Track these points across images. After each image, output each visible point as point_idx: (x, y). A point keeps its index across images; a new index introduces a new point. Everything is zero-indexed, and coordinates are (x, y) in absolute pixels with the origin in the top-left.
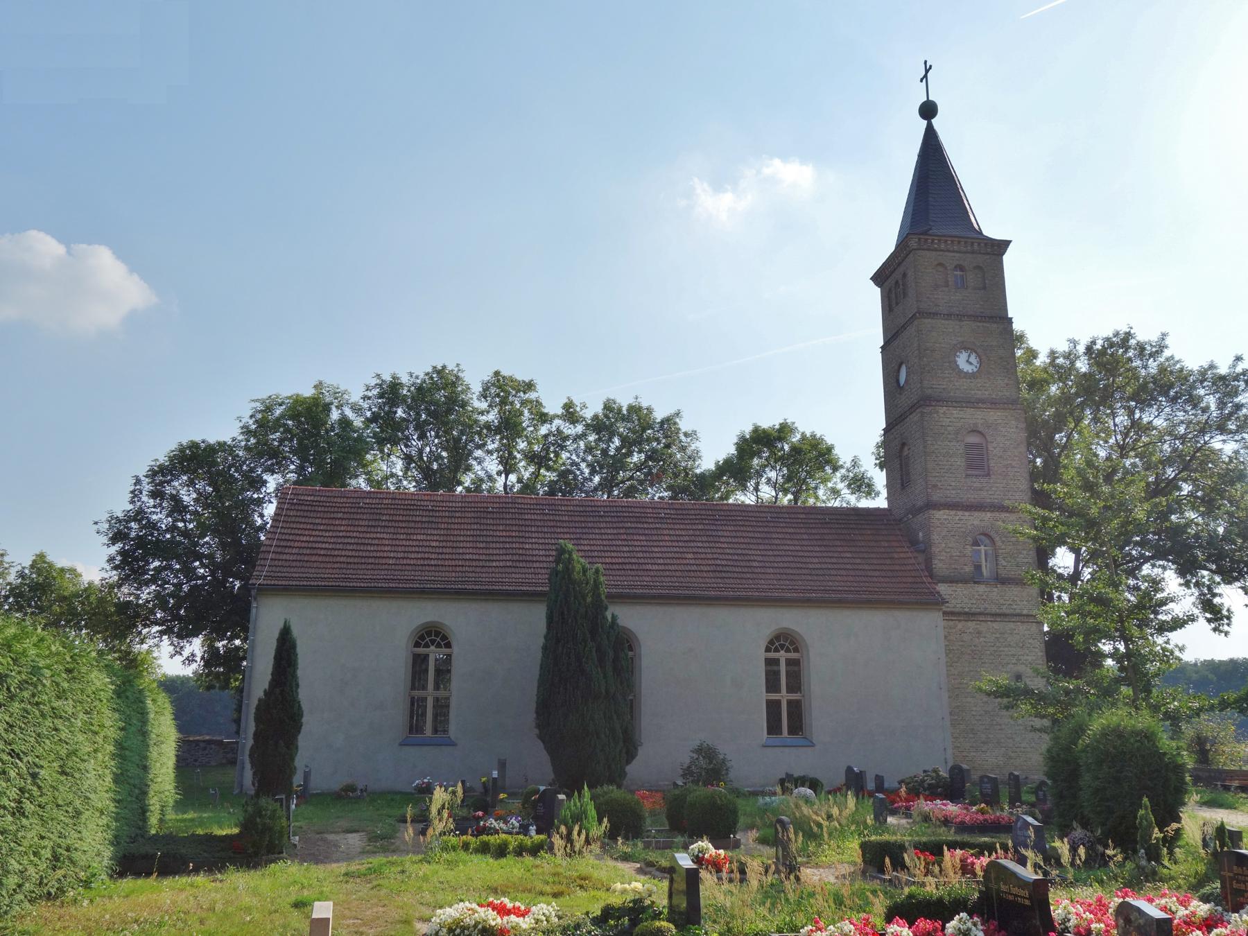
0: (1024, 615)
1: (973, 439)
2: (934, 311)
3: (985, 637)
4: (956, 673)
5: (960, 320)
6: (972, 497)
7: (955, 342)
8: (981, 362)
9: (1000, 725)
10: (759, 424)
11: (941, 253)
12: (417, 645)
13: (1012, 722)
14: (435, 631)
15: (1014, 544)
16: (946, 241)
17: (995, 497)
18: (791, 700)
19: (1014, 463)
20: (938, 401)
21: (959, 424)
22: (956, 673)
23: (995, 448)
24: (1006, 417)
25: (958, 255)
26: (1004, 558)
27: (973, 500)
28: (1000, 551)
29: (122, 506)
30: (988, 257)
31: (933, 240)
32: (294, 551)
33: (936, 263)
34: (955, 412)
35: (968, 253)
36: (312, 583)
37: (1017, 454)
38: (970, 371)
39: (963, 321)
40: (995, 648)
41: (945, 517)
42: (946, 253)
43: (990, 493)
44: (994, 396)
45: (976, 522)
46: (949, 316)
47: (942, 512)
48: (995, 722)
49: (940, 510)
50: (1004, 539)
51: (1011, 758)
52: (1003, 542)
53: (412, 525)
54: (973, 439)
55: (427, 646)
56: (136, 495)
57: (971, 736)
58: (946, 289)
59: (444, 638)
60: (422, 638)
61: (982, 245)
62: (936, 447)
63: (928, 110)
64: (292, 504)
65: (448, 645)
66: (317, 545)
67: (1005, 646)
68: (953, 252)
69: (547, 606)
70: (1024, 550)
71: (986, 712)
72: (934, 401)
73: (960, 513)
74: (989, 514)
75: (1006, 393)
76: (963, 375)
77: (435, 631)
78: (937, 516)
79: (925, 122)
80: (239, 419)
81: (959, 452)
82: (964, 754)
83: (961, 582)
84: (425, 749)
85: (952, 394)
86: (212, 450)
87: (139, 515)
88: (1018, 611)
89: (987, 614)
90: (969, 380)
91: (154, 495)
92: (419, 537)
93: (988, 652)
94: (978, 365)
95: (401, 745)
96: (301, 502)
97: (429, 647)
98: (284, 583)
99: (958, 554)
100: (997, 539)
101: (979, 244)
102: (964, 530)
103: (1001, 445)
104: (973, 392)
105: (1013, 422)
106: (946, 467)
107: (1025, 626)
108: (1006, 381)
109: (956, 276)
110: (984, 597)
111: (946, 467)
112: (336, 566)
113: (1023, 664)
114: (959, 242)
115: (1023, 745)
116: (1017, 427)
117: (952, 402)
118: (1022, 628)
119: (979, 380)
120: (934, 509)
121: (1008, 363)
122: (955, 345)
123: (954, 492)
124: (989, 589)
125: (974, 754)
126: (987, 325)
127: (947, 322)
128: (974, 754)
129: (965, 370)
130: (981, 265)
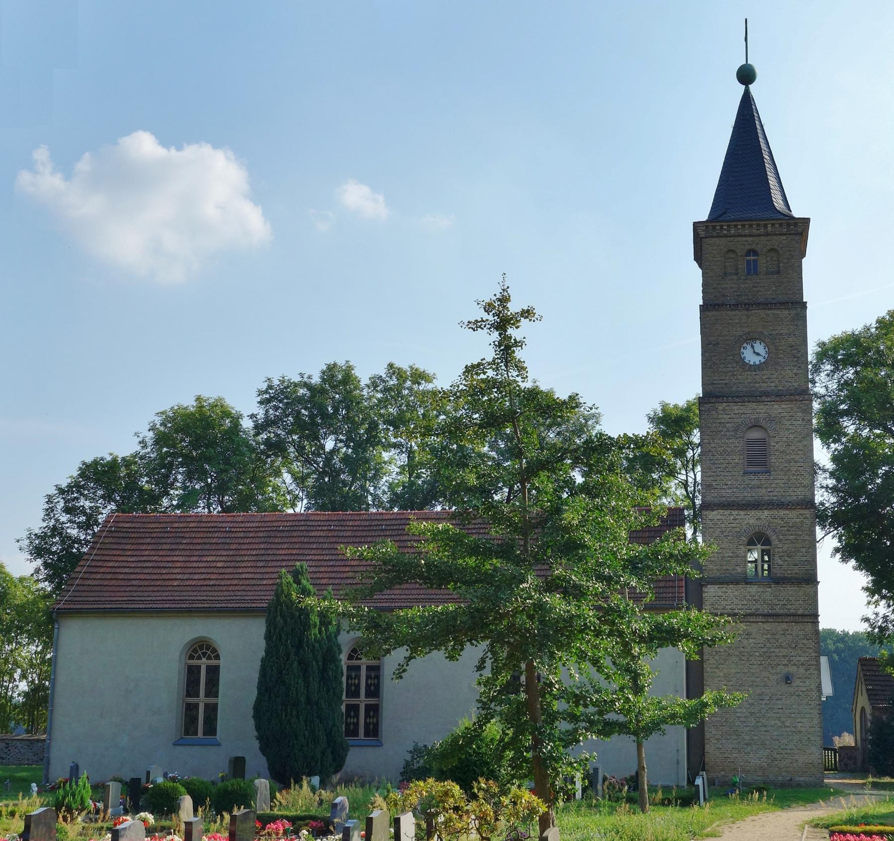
0: (799, 615)
1: (755, 435)
2: (720, 302)
3: (755, 639)
4: (722, 674)
5: (748, 310)
6: (748, 496)
7: (741, 333)
8: (769, 353)
9: (766, 726)
10: (667, 401)
11: (732, 239)
12: (191, 657)
13: (779, 724)
14: (207, 645)
15: (792, 543)
16: (736, 226)
17: (775, 493)
18: (370, 705)
19: (797, 458)
20: (718, 397)
21: (739, 420)
22: (722, 674)
23: (777, 443)
24: (792, 409)
25: (751, 239)
26: (780, 557)
27: (750, 499)
28: (777, 550)
29: (38, 525)
30: (784, 237)
31: (722, 227)
32: (99, 576)
33: (725, 250)
34: (736, 408)
35: (762, 235)
36: (100, 606)
37: (801, 448)
38: (757, 363)
39: (751, 310)
40: (765, 650)
41: (719, 517)
42: (737, 239)
43: (769, 490)
44: (781, 388)
45: (752, 521)
46: (736, 306)
47: (715, 512)
48: (760, 724)
49: (713, 510)
50: (781, 537)
51: (775, 759)
52: (780, 540)
53: (207, 547)
54: (755, 435)
55: (199, 658)
56: (49, 512)
57: (735, 737)
58: (735, 277)
59: (215, 650)
60: (195, 651)
61: (777, 226)
62: (713, 445)
63: (746, 75)
64: (111, 531)
65: (217, 657)
66: (118, 570)
67: (777, 647)
68: (745, 236)
69: (267, 621)
70: (803, 547)
71: (751, 713)
72: (713, 398)
73: (735, 513)
74: (766, 512)
75: (794, 384)
76: (747, 368)
77: (207, 645)
78: (710, 517)
79: (742, 88)
80: (137, 434)
81: (738, 449)
82: (727, 755)
83: (732, 583)
84: (196, 748)
85: (734, 389)
86: (113, 465)
87: (56, 530)
88: (792, 611)
89: (759, 615)
90: (754, 373)
91: (67, 510)
92: (209, 559)
93: (758, 654)
94: (766, 356)
95: (175, 744)
96: (119, 530)
97: (201, 659)
98: (77, 606)
99: (731, 554)
100: (774, 537)
101: (773, 225)
102: (738, 529)
103: (784, 439)
104: (757, 385)
105: (799, 414)
106: (723, 466)
107: (799, 626)
108: (795, 371)
109: (748, 262)
110: (757, 597)
111: (723, 466)
112: (128, 589)
113: (795, 665)
114: (751, 226)
115: (789, 747)
116: (803, 419)
117: (733, 397)
118: (796, 629)
119: (765, 372)
120: (707, 510)
121: (799, 351)
122: (741, 336)
123: (730, 491)
124: (762, 590)
125: (737, 755)
126: (778, 312)
127: (733, 313)
128: (737, 755)
129: (752, 363)
130: (776, 247)
